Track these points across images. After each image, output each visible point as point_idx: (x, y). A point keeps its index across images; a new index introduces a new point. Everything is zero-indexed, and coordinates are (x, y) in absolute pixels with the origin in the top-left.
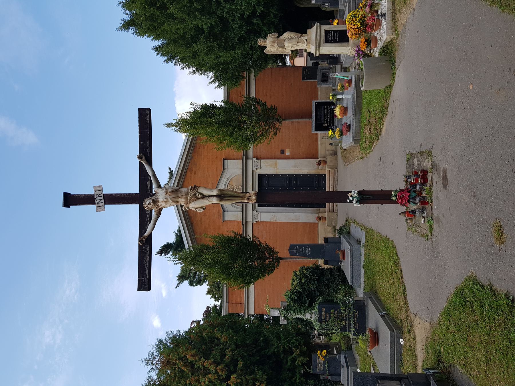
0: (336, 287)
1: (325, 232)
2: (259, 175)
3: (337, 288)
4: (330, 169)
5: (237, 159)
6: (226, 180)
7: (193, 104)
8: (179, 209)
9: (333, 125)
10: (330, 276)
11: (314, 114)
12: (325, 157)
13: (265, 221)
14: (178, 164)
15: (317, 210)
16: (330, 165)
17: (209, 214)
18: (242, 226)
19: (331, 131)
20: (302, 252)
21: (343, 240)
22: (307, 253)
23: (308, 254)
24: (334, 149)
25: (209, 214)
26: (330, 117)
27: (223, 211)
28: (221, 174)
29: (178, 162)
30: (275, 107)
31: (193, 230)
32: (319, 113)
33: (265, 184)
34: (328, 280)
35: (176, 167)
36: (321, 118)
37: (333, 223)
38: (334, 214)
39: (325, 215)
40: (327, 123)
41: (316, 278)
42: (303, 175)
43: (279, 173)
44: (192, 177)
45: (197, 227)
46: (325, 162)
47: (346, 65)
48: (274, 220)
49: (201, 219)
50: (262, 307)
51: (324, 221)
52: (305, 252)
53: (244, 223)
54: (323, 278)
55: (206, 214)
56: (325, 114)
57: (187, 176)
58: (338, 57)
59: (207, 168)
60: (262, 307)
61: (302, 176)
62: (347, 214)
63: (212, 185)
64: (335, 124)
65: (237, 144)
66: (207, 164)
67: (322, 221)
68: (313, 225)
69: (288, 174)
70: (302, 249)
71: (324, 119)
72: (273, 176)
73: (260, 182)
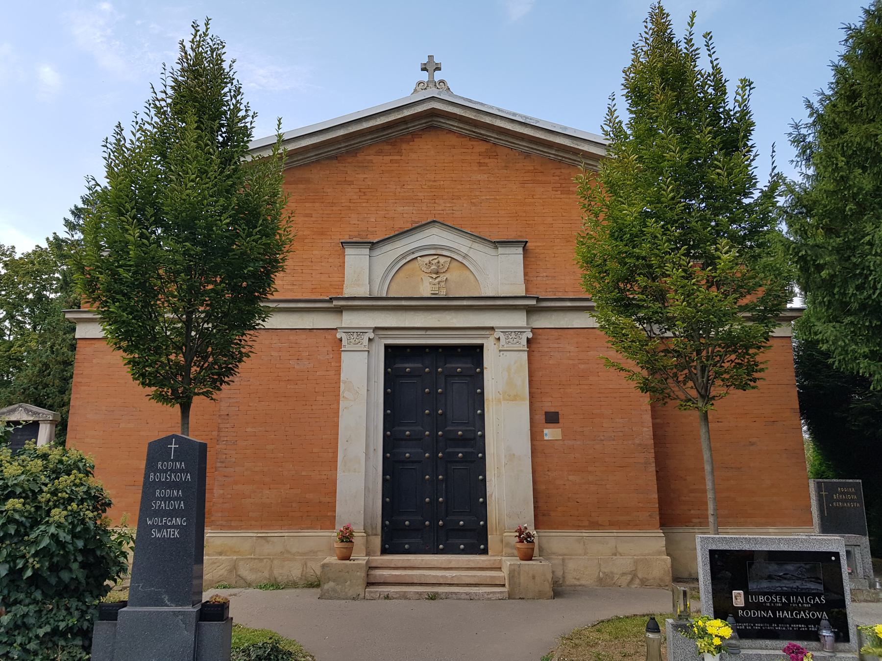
2: (481, 347)
4: (507, 585)
5: (527, 281)
6: (464, 250)
8: (378, 120)
10: (41, 632)
13: (343, 365)
14: (508, 113)
15: (376, 527)
16: (519, 574)
20: (164, 499)
22: (157, 520)
23: (153, 526)
29: (515, 115)
30: (754, 380)
32: (790, 567)
35: (499, 110)
36: (770, 578)
37: (331, 584)
38: (360, 589)
39: (360, 559)
40: (748, 606)
41: (25, 568)
42: (482, 480)
44: (469, 157)
45: (328, 172)
49: (351, 183)
50: (94, 361)
51: (338, 551)
53: (335, 303)
54: (35, 602)
55: (364, 197)
56: (788, 599)
60: (94, 361)
61: (481, 477)
63: (449, 212)
65: (606, 245)
66: (510, 197)
67: (337, 545)
68: (329, 514)
71: (764, 594)
72: (479, 391)
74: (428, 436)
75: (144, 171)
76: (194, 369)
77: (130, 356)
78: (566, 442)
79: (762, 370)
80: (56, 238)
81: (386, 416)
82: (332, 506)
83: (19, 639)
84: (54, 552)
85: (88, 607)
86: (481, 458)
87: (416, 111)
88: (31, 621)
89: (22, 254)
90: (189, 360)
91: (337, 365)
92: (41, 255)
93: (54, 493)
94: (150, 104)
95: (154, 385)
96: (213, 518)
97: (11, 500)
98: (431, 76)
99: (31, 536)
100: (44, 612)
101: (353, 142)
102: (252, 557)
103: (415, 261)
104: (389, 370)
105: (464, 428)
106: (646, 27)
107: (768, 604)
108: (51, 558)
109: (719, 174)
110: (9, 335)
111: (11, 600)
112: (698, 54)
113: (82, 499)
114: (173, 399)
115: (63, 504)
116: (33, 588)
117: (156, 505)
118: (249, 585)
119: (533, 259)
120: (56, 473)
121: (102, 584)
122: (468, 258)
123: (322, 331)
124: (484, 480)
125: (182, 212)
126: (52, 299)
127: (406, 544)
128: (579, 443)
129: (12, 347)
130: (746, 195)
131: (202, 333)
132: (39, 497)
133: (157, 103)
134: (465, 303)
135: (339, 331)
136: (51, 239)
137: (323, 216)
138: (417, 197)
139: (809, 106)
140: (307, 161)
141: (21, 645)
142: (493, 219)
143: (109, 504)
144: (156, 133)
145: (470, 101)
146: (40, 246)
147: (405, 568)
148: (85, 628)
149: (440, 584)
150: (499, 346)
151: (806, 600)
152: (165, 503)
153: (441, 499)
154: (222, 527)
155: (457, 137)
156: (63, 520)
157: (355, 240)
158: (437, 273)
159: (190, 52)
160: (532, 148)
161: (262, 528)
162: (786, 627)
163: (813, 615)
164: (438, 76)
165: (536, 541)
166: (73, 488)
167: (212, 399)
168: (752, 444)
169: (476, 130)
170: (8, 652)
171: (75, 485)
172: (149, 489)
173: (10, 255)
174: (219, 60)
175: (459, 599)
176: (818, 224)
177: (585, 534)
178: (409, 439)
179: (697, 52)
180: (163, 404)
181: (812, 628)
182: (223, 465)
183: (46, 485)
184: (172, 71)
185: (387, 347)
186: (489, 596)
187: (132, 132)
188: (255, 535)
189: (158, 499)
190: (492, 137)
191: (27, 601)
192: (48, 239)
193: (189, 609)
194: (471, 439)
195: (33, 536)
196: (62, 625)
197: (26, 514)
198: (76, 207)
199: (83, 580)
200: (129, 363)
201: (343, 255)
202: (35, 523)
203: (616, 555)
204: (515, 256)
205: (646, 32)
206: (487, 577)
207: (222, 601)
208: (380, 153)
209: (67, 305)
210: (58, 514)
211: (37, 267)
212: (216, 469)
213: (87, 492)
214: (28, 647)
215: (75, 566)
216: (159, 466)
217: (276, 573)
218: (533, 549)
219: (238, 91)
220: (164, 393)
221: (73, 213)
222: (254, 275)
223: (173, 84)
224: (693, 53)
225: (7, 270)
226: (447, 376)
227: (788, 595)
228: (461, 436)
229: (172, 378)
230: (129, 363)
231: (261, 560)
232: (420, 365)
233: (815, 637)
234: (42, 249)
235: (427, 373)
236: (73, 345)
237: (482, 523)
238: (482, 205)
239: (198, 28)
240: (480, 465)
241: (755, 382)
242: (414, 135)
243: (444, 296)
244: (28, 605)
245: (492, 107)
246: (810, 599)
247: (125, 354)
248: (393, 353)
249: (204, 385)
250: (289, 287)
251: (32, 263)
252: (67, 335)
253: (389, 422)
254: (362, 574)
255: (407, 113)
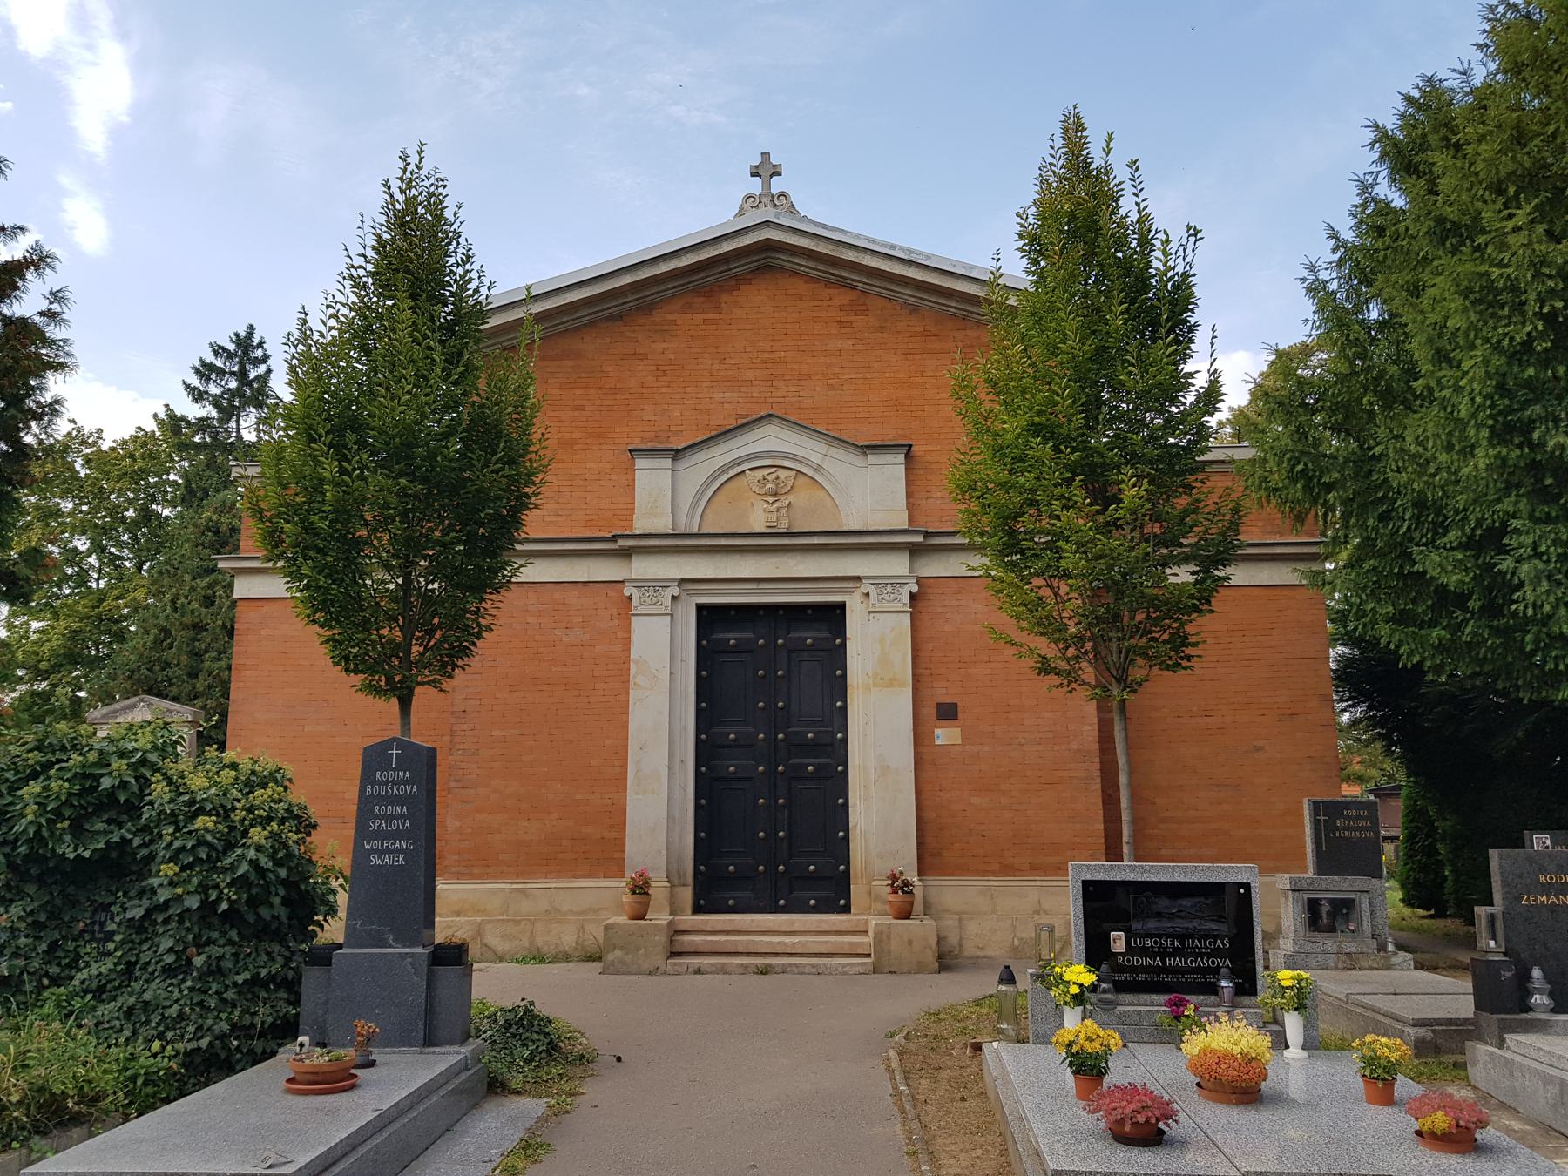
0: (164, 1018)
1: (581, 913)
2: (842, 607)
3: (158, 1024)
4: (871, 933)
5: (910, 506)
6: (816, 459)
7: (1193, 239)
8: (684, 258)
9: (1120, 988)
10: (240, 979)
11: (1178, 877)
12: (928, 908)
13: (635, 637)
16: (889, 937)
17: (664, 390)
18: (609, 535)
19: (1088, 978)
21: (444, 1060)
22: (376, 844)
23: (371, 851)
24: (966, 954)
25: (664, 390)
26: (1165, 970)
27: (677, 451)
28: (842, 438)
29: (893, 247)
30: (1189, 658)
31: (593, 323)
32: (1186, 902)
33: (801, 635)
34: (215, 971)
35: (869, 240)
36: (1159, 915)
37: (618, 953)
38: (659, 960)
39: (659, 917)
41: (219, 899)
42: (843, 805)
43: (852, 700)
44: (824, 314)
45: (608, 340)
46: (905, 913)
47: (1480, 1066)
48: (634, 677)
49: (644, 357)
51: (627, 907)
52: (380, 835)
53: (621, 543)
54: (231, 942)
55: (664, 379)
56: (1182, 943)
57: (831, 291)
58: (1530, 1016)
59: (868, 376)
61: (841, 801)
62: (619, 1059)
64: (1127, 997)
65: (993, 472)
66: (887, 375)
67: (627, 897)
68: (616, 855)
69: (845, 740)
70: (401, 817)
71: (1151, 936)
72: (839, 672)
73: (810, 612)
74: (763, 740)
75: (417, 633)
76: (414, 649)
77: (328, 633)
78: (967, 748)
79: (1195, 645)
80: (171, 415)
81: (699, 712)
82: (620, 844)
83: (214, 987)
84: (253, 882)
85: (293, 953)
86: (842, 772)
87: (742, 245)
88: (227, 964)
89: (114, 441)
90: (409, 637)
91: (625, 635)
92: (145, 444)
93: (250, 810)
94: (344, 278)
95: (362, 672)
96: (445, 864)
97: (200, 818)
98: (767, 185)
99: (225, 862)
100: (242, 956)
101: (646, 293)
102: (505, 917)
103: (741, 476)
104: (704, 642)
105: (817, 729)
106: (1052, 148)
107: (1156, 950)
108: (249, 889)
109: (1130, 373)
110: (97, 580)
111: (204, 939)
112: (1122, 190)
113: (283, 818)
114: (387, 690)
115: (261, 824)
116: (227, 926)
117: (374, 825)
118: (501, 959)
119: (921, 472)
120: (249, 786)
121: (307, 929)
122: (822, 470)
123: (602, 585)
124: (846, 805)
125: (393, 438)
126: (167, 518)
127: (731, 898)
128: (986, 748)
129: (103, 600)
130: (1174, 401)
131: (427, 597)
132: (232, 815)
133: (353, 272)
134: (816, 540)
135: (627, 584)
136: (162, 415)
137: (602, 408)
138: (744, 378)
139: (1334, 235)
140: (577, 323)
141: (217, 993)
142: (860, 409)
143: (315, 826)
144: (354, 318)
145: (825, 227)
146: (143, 427)
147: (727, 932)
148: (290, 977)
149: (776, 954)
150: (868, 605)
151: (1205, 944)
152: (386, 823)
153: (781, 834)
154: (459, 876)
155: (806, 282)
156: (263, 842)
157: (650, 445)
158: (775, 494)
159: (398, 196)
160: (921, 299)
161: (517, 876)
162: (1178, 979)
163: (1213, 962)
164: (777, 185)
165: (918, 892)
166: (272, 805)
167: (441, 690)
168: (1260, 749)
169: (835, 272)
170: (203, 1001)
171: (273, 801)
172: (366, 806)
173: (96, 443)
174: (439, 217)
175: (802, 974)
176: (1326, 423)
177: (994, 882)
178: (735, 745)
179: (1120, 187)
180: (374, 697)
181: (1210, 978)
182: (460, 785)
183: (239, 801)
184: (372, 224)
185: (700, 608)
186: (845, 969)
187: (322, 320)
188: (509, 886)
189: (377, 817)
190: (859, 282)
191: (221, 942)
192: (155, 416)
193: (420, 950)
194: (825, 746)
195: (227, 861)
196: (264, 972)
197: (218, 835)
198: (201, 360)
199: (284, 919)
200: (327, 641)
201: (631, 469)
202: (230, 846)
203: (1039, 914)
204: (895, 466)
205: (1051, 155)
206: (843, 943)
207: (459, 942)
208: (687, 308)
209: (196, 530)
210: (257, 835)
211: (139, 464)
212: (449, 791)
213: (288, 810)
214: (225, 995)
215: (277, 901)
216: (378, 776)
217: (539, 940)
218: (912, 903)
219: (468, 258)
220: (375, 682)
221: (197, 371)
222: (497, 517)
223: (375, 243)
224: (1115, 189)
225: (90, 468)
226: (790, 652)
227: (1181, 938)
228: (812, 739)
229: (385, 661)
230: (327, 641)
231: (517, 922)
232: (750, 635)
233: (1213, 989)
234: (147, 433)
235: (761, 646)
236: (208, 598)
237: (842, 868)
238: (844, 388)
239: (408, 160)
240: (840, 783)
241: (1189, 661)
242: (740, 280)
243: (785, 531)
244: (223, 946)
245: (858, 236)
246: (1210, 943)
247: (321, 631)
248: (709, 617)
249: (429, 671)
250: (553, 519)
251: (132, 456)
252: (198, 581)
253: (705, 720)
254: (661, 939)
255: (728, 247)
